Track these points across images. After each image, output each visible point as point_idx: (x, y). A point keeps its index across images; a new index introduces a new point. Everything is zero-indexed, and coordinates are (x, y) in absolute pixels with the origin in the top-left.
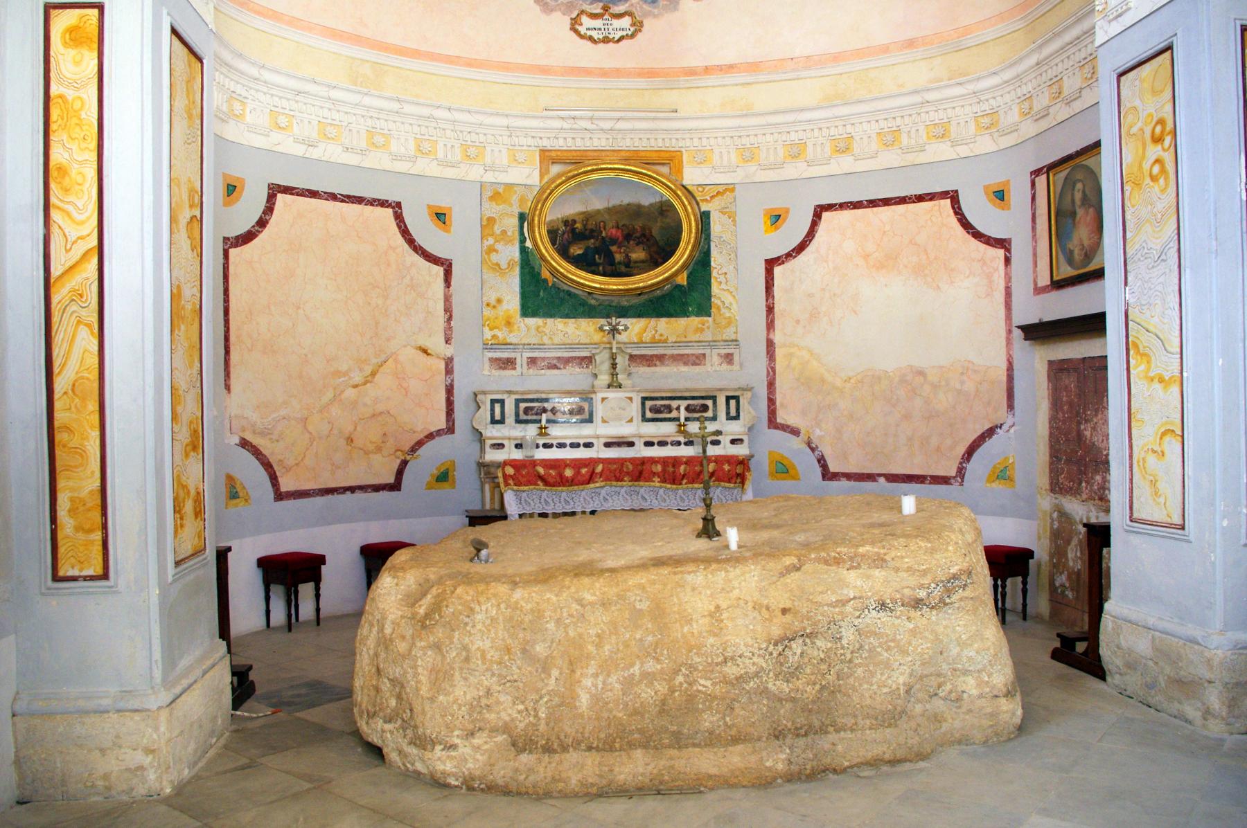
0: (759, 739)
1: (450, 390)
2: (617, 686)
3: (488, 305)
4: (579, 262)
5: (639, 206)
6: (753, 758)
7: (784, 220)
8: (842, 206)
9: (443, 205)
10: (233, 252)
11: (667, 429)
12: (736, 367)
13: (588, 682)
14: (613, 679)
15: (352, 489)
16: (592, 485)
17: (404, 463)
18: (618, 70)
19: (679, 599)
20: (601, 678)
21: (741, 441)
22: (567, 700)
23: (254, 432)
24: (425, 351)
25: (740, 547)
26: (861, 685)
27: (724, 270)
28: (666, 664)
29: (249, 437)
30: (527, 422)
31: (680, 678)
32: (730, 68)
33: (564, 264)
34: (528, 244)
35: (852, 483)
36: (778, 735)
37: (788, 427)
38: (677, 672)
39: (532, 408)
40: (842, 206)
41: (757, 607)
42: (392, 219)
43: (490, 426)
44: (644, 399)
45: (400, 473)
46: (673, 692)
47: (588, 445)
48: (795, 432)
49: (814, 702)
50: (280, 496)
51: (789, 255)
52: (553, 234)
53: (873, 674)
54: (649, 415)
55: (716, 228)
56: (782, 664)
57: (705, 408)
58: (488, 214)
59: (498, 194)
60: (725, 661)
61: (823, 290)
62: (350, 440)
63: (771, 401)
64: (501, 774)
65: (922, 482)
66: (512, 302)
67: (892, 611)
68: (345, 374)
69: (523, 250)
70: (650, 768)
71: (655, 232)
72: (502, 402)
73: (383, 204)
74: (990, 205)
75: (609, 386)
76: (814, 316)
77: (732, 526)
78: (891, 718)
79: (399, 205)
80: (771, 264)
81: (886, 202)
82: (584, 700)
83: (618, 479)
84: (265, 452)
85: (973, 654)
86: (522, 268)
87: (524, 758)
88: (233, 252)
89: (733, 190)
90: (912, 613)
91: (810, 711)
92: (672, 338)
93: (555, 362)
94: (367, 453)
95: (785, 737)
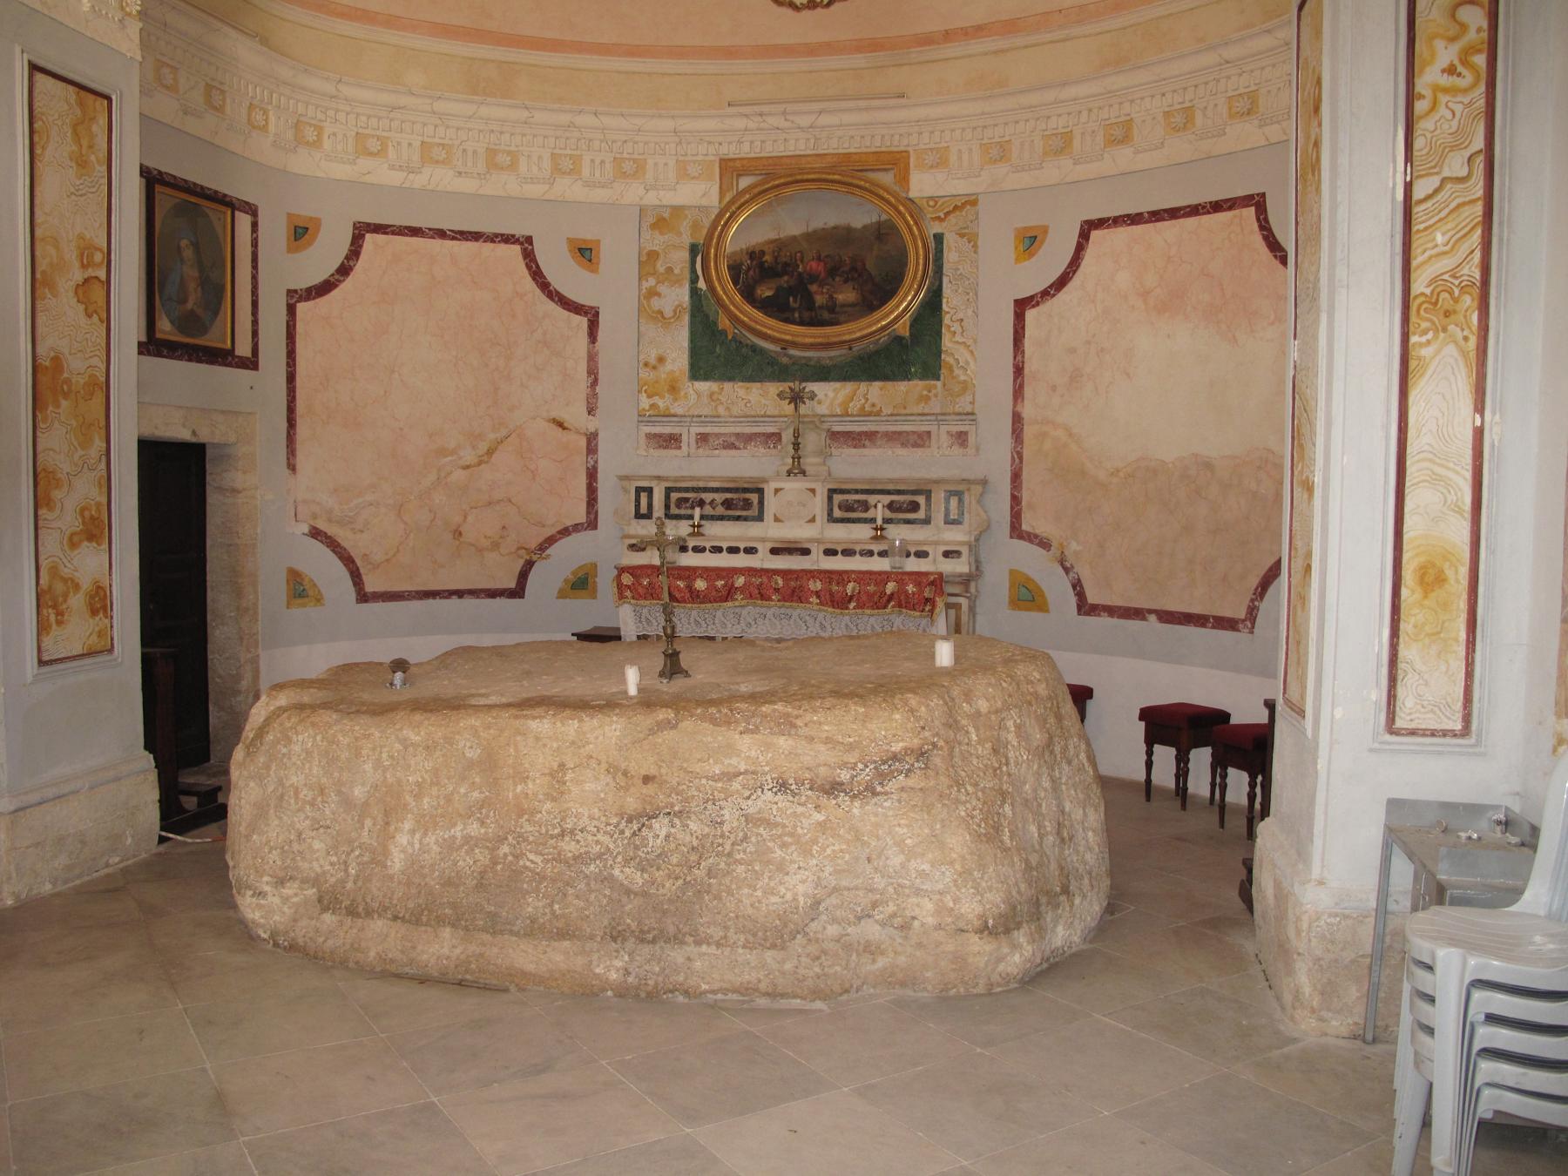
0: (592, 937)
1: (592, 475)
2: (435, 848)
3: (646, 365)
4: (766, 306)
5: (849, 230)
6: (580, 962)
7: (1042, 243)
8: (1117, 221)
9: (589, 237)
10: (302, 308)
11: (860, 533)
12: (971, 451)
13: (403, 839)
14: (431, 839)
15: (460, 594)
16: (730, 604)
17: (529, 565)
18: (828, 44)
19: (517, 750)
20: (417, 836)
21: (958, 554)
22: (379, 857)
23: (330, 520)
24: (561, 425)
25: (640, 690)
26: (739, 888)
27: (961, 315)
28: (492, 829)
29: (322, 525)
30: (678, 517)
31: (505, 849)
32: (979, 31)
33: (748, 308)
34: (702, 284)
35: (1115, 621)
36: (616, 935)
37: (1036, 536)
38: (503, 839)
39: (686, 500)
40: (1117, 221)
41: (612, 770)
42: (521, 257)
43: (634, 522)
44: (832, 492)
45: (523, 576)
46: (496, 863)
47: (750, 551)
48: (1045, 544)
49: (670, 901)
50: (363, 597)
51: (1046, 294)
52: (735, 270)
53: (758, 876)
54: (837, 513)
55: (950, 257)
56: (637, 848)
57: (915, 507)
58: (650, 247)
59: (663, 221)
60: (562, 834)
61: (1089, 342)
62: (458, 533)
63: (1016, 500)
64: (301, 933)
65: (1203, 625)
66: (679, 360)
67: (794, 794)
68: (453, 452)
69: (694, 292)
70: (458, 951)
71: (870, 265)
72: (650, 491)
73: (508, 239)
74: (572, 262)
75: (789, 473)
76: (1075, 378)
77: (632, 664)
78: (778, 934)
79: (529, 240)
80: (1022, 306)
81: (1174, 213)
82: (397, 862)
83: (763, 597)
84: (344, 544)
85: (926, 867)
86: (693, 316)
87: (328, 918)
88: (302, 308)
89: (974, 203)
90: (824, 800)
91: (665, 912)
92: (887, 410)
93: (733, 439)
94: (480, 550)
95: (625, 940)
